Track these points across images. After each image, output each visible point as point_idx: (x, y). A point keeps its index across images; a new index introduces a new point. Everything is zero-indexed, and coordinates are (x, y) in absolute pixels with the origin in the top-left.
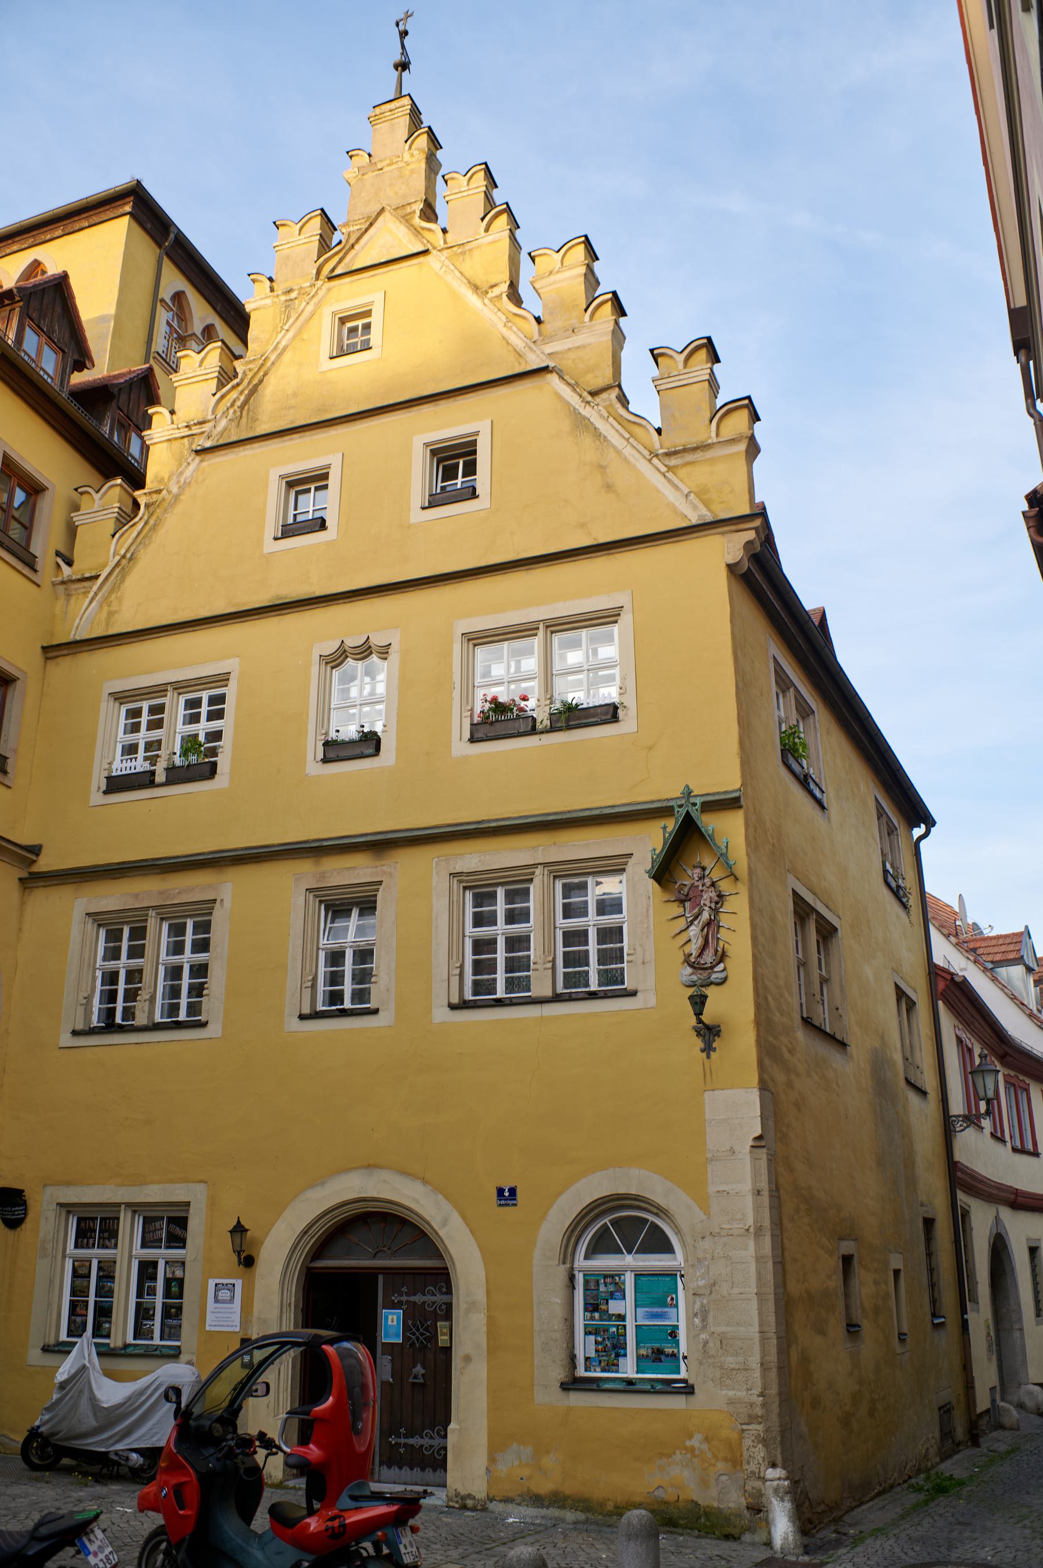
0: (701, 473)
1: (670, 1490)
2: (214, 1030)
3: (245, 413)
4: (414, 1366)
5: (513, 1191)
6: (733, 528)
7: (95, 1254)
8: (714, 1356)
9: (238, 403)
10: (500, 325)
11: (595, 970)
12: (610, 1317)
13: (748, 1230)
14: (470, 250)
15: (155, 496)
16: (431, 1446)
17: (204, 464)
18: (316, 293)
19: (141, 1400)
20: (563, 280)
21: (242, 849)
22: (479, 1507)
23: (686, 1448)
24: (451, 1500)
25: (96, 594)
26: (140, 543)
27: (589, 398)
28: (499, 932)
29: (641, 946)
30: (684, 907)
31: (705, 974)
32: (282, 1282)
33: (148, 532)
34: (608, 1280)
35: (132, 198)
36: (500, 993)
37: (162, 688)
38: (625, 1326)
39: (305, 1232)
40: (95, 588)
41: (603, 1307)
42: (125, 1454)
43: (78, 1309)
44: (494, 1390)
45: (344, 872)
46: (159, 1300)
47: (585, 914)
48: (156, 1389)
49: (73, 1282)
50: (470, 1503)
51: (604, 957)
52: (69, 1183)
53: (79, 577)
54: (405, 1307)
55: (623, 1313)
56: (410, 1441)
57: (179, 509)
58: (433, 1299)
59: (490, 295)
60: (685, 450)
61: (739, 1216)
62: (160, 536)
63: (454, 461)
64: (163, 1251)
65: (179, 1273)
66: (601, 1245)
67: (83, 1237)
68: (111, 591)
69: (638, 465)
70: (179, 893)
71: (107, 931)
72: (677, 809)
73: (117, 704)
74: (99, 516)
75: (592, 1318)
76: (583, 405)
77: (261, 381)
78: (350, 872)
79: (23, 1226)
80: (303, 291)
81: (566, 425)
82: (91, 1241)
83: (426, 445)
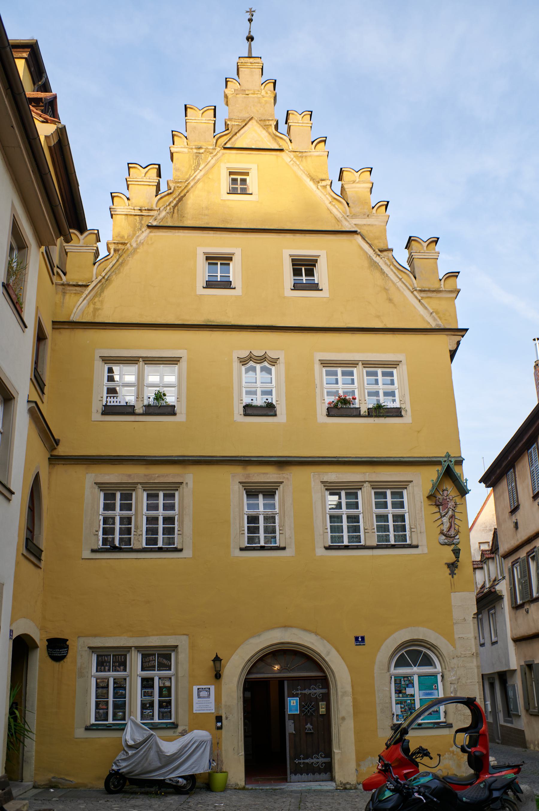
0: (433, 303)
1: (444, 770)
2: (187, 553)
3: (176, 211)
4: (307, 725)
5: (363, 638)
6: (453, 333)
7: (111, 675)
8: (460, 710)
9: (173, 204)
10: (327, 202)
11: (395, 536)
12: (407, 696)
13: (473, 654)
14: (306, 156)
15: (120, 246)
16: (318, 763)
17: (152, 234)
18: (217, 154)
19: (185, 750)
20: (359, 188)
21: (197, 456)
22: (353, 788)
23: (450, 752)
24: (339, 786)
25: (87, 296)
26: (113, 272)
27: (379, 253)
28: (161, 514)
29: (419, 524)
30: (439, 508)
31: (451, 539)
32: (238, 686)
33: (118, 266)
34: (405, 679)
35: (29, 50)
36: (160, 544)
37: (136, 359)
38: (414, 700)
39: (249, 660)
40: (87, 292)
41: (404, 691)
42: (175, 779)
43: (100, 706)
44: (357, 733)
45: (264, 475)
46: (156, 699)
47: (114, 510)
48: (193, 744)
49: (96, 691)
50: (348, 786)
51: (166, 531)
52: (95, 636)
53: (75, 283)
54: (300, 696)
55: (413, 693)
56: (306, 761)
57: (136, 257)
58: (315, 691)
59: (320, 184)
60: (429, 291)
61: (469, 648)
62: (126, 269)
63: (304, 267)
64: (156, 672)
65: (167, 684)
66: (401, 662)
67: (101, 665)
68: (95, 296)
69: (405, 293)
70: (158, 476)
71: (121, 494)
72: (443, 463)
73: (104, 363)
74: (84, 249)
75: (399, 697)
76: (375, 255)
77: (185, 195)
78: (269, 475)
79: (65, 660)
80: (207, 150)
81: (366, 264)
82: (107, 668)
83: (291, 256)
